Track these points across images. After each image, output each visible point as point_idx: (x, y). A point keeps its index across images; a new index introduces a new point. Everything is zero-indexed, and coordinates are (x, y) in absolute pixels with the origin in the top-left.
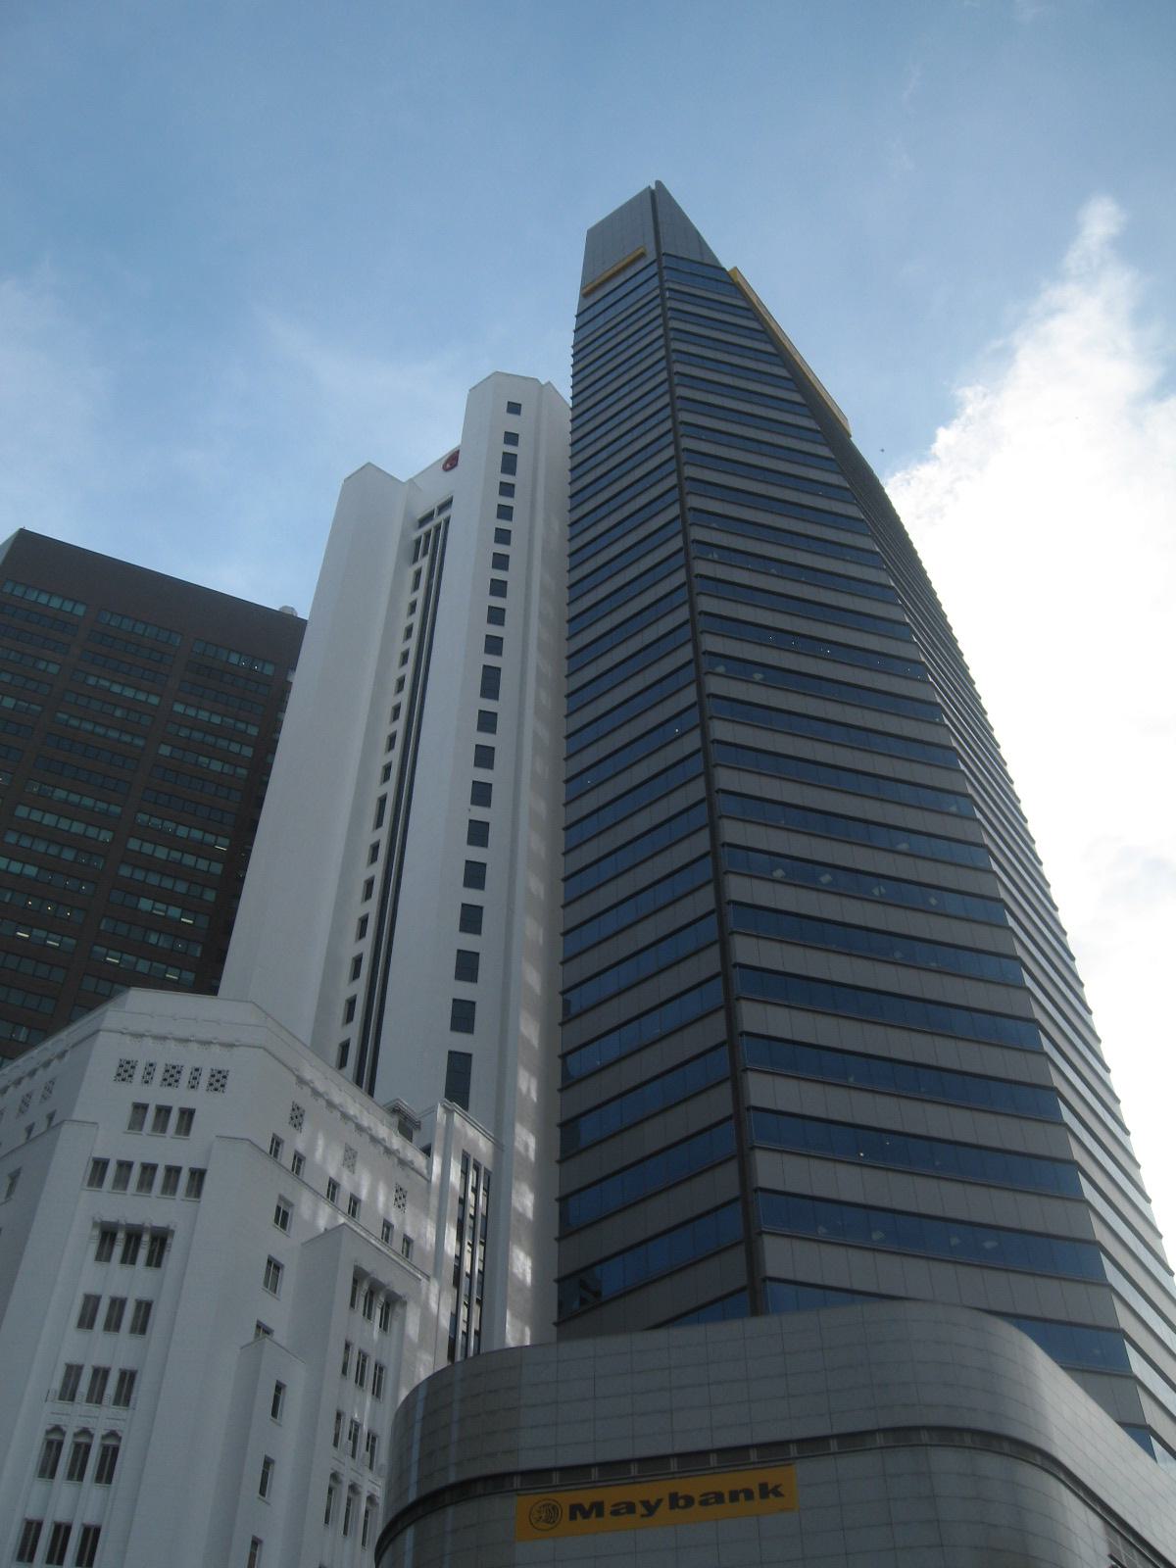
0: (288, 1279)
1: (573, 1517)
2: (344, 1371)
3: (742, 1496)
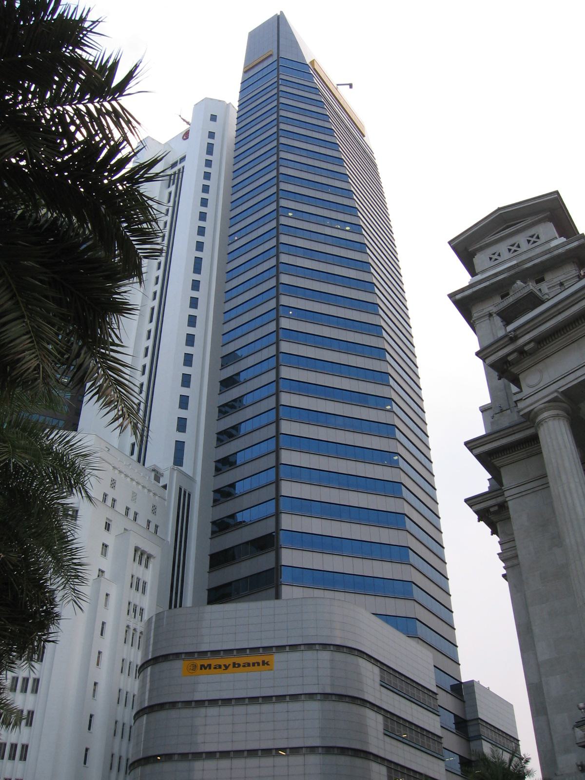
0: (110, 550)
1: (201, 669)
2: (131, 587)
3: (256, 664)
